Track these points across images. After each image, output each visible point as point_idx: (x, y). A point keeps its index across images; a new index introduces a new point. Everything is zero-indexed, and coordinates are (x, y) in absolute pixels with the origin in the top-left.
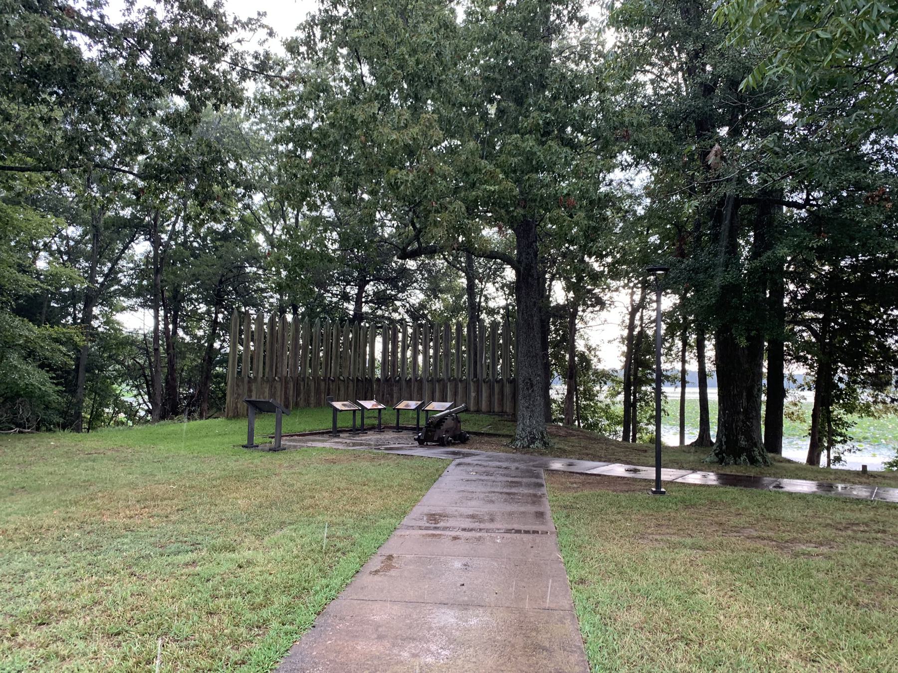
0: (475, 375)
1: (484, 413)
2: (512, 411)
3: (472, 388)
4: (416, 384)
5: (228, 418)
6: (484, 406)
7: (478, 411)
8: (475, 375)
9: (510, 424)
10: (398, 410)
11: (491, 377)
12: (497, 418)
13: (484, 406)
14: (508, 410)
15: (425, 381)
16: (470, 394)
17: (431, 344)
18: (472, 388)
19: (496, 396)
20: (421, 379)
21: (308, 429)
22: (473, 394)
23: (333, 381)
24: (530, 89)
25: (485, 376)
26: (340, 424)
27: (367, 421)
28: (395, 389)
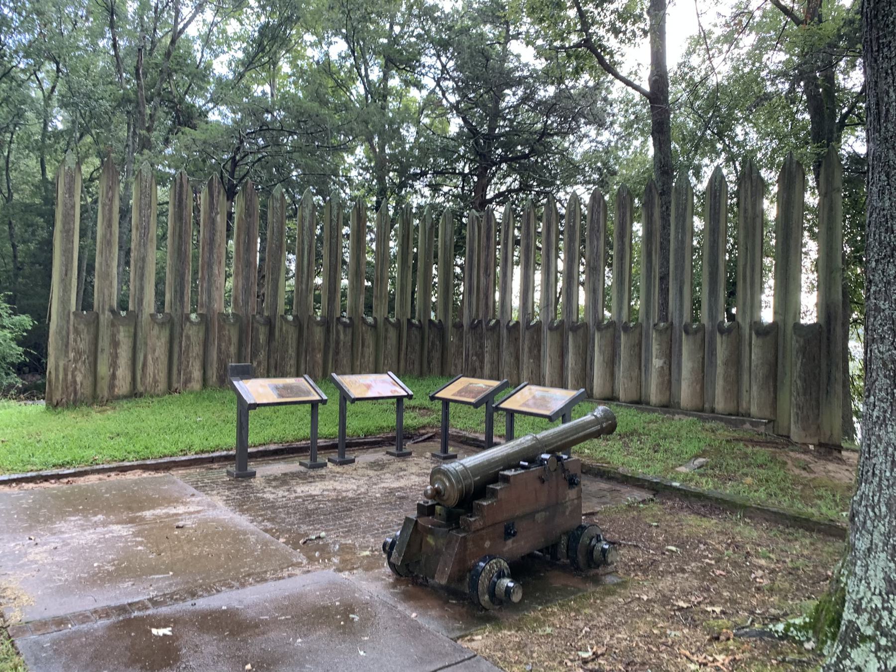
0: (664, 317)
1: (686, 413)
2: (767, 413)
3: (655, 348)
4: (528, 335)
5: (54, 406)
6: (686, 394)
7: (669, 406)
8: (664, 317)
9: (763, 453)
10: (446, 402)
11: (704, 315)
12: (724, 433)
13: (686, 394)
14: (754, 410)
15: (545, 328)
16: (648, 361)
17: (561, 244)
18: (655, 348)
19: (720, 370)
20: (539, 323)
21: (747, 348)
22: (657, 363)
23: (345, 325)
24: (712, 604)
25: (687, 317)
26: (256, 438)
27: (354, 425)
28: (488, 345)
